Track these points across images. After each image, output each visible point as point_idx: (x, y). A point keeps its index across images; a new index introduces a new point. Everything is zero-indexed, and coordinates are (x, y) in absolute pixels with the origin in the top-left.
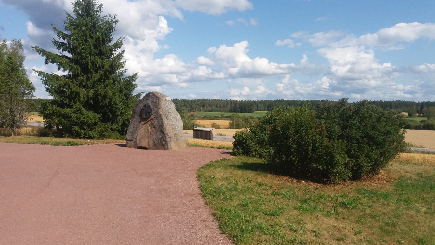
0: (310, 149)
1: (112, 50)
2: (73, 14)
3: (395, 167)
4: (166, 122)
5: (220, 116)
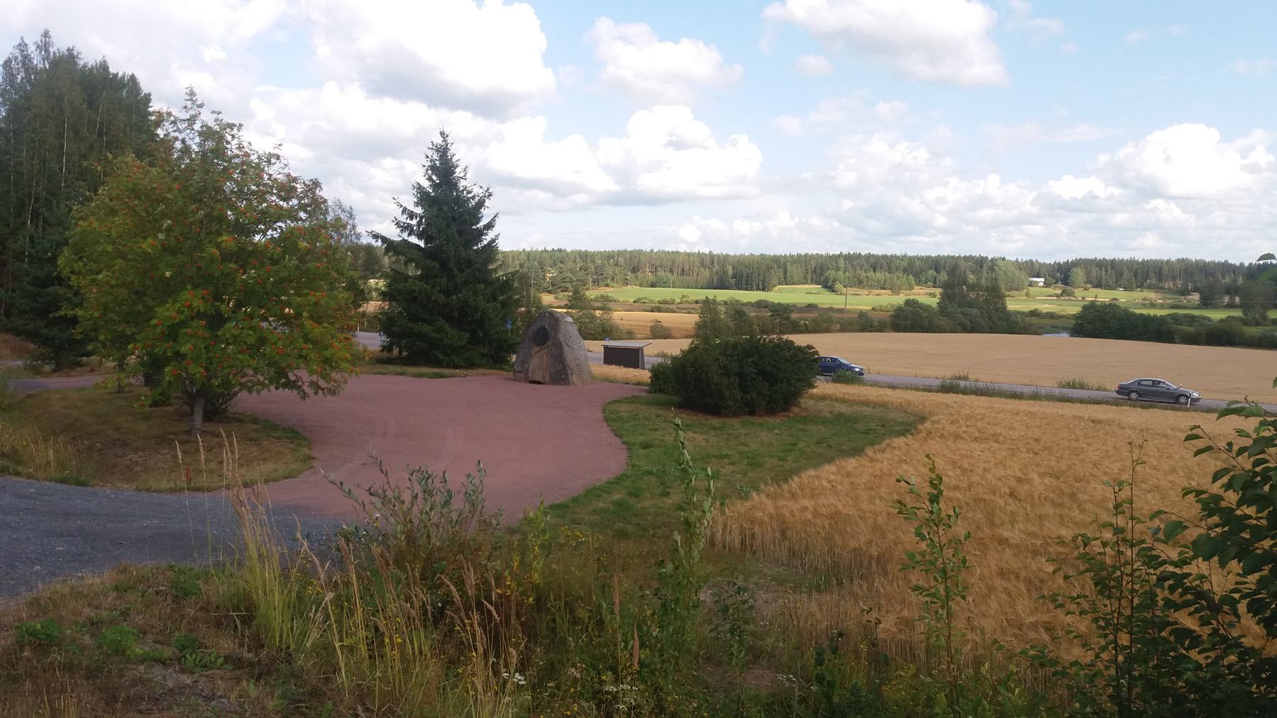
1: (480, 233)
2: (426, 184)
4: (566, 349)
5: (678, 301)
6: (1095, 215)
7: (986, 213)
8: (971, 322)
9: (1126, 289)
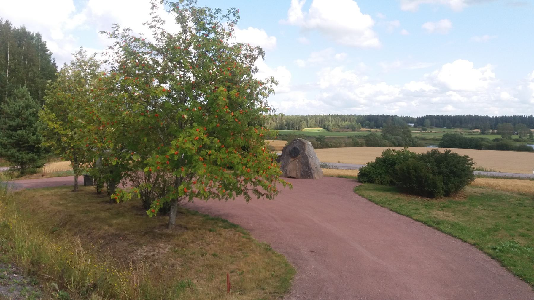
0: (424, 180)
3: (468, 189)
4: (310, 159)
6: (425, 98)
7: (381, 98)
8: (398, 142)
9: (448, 127)
